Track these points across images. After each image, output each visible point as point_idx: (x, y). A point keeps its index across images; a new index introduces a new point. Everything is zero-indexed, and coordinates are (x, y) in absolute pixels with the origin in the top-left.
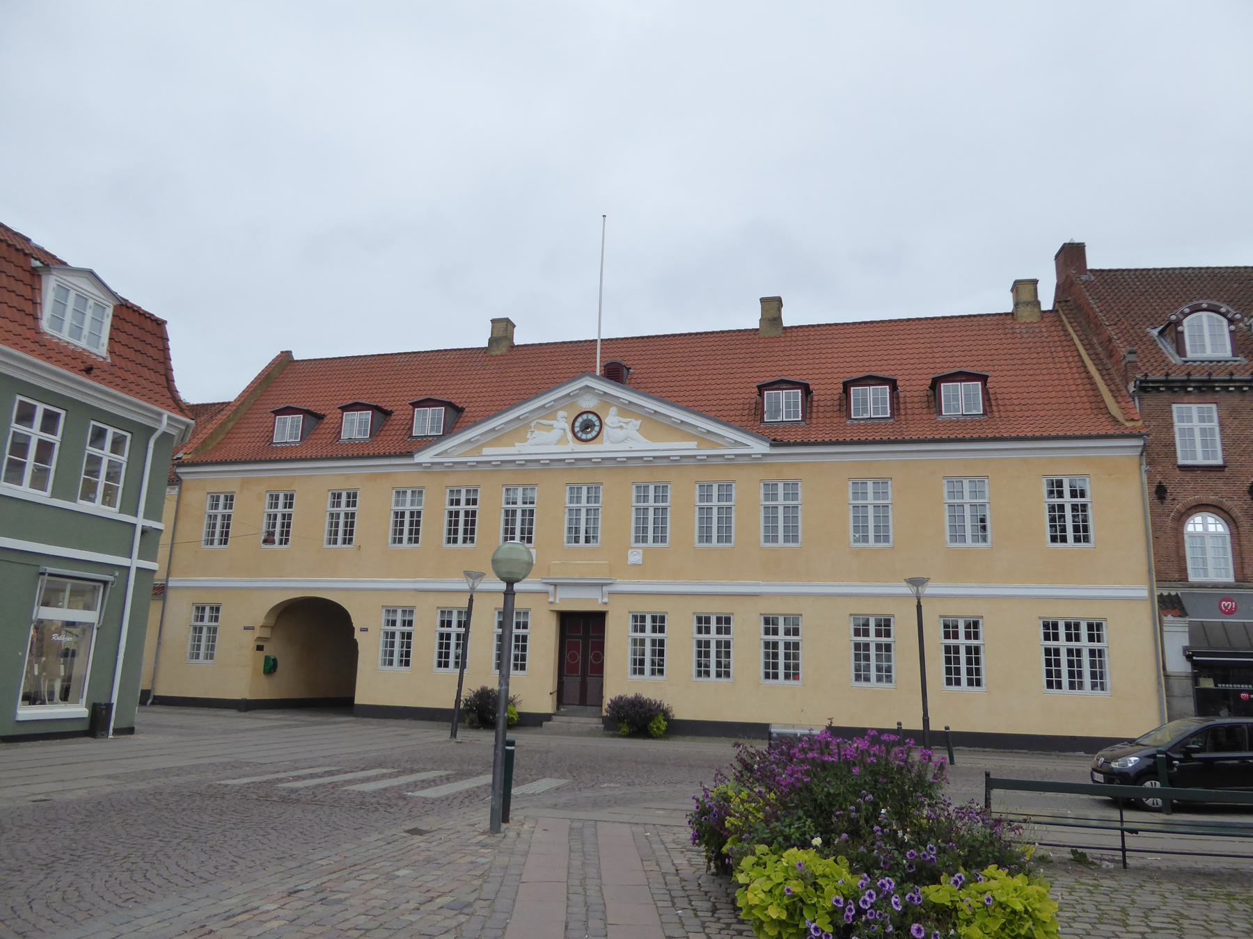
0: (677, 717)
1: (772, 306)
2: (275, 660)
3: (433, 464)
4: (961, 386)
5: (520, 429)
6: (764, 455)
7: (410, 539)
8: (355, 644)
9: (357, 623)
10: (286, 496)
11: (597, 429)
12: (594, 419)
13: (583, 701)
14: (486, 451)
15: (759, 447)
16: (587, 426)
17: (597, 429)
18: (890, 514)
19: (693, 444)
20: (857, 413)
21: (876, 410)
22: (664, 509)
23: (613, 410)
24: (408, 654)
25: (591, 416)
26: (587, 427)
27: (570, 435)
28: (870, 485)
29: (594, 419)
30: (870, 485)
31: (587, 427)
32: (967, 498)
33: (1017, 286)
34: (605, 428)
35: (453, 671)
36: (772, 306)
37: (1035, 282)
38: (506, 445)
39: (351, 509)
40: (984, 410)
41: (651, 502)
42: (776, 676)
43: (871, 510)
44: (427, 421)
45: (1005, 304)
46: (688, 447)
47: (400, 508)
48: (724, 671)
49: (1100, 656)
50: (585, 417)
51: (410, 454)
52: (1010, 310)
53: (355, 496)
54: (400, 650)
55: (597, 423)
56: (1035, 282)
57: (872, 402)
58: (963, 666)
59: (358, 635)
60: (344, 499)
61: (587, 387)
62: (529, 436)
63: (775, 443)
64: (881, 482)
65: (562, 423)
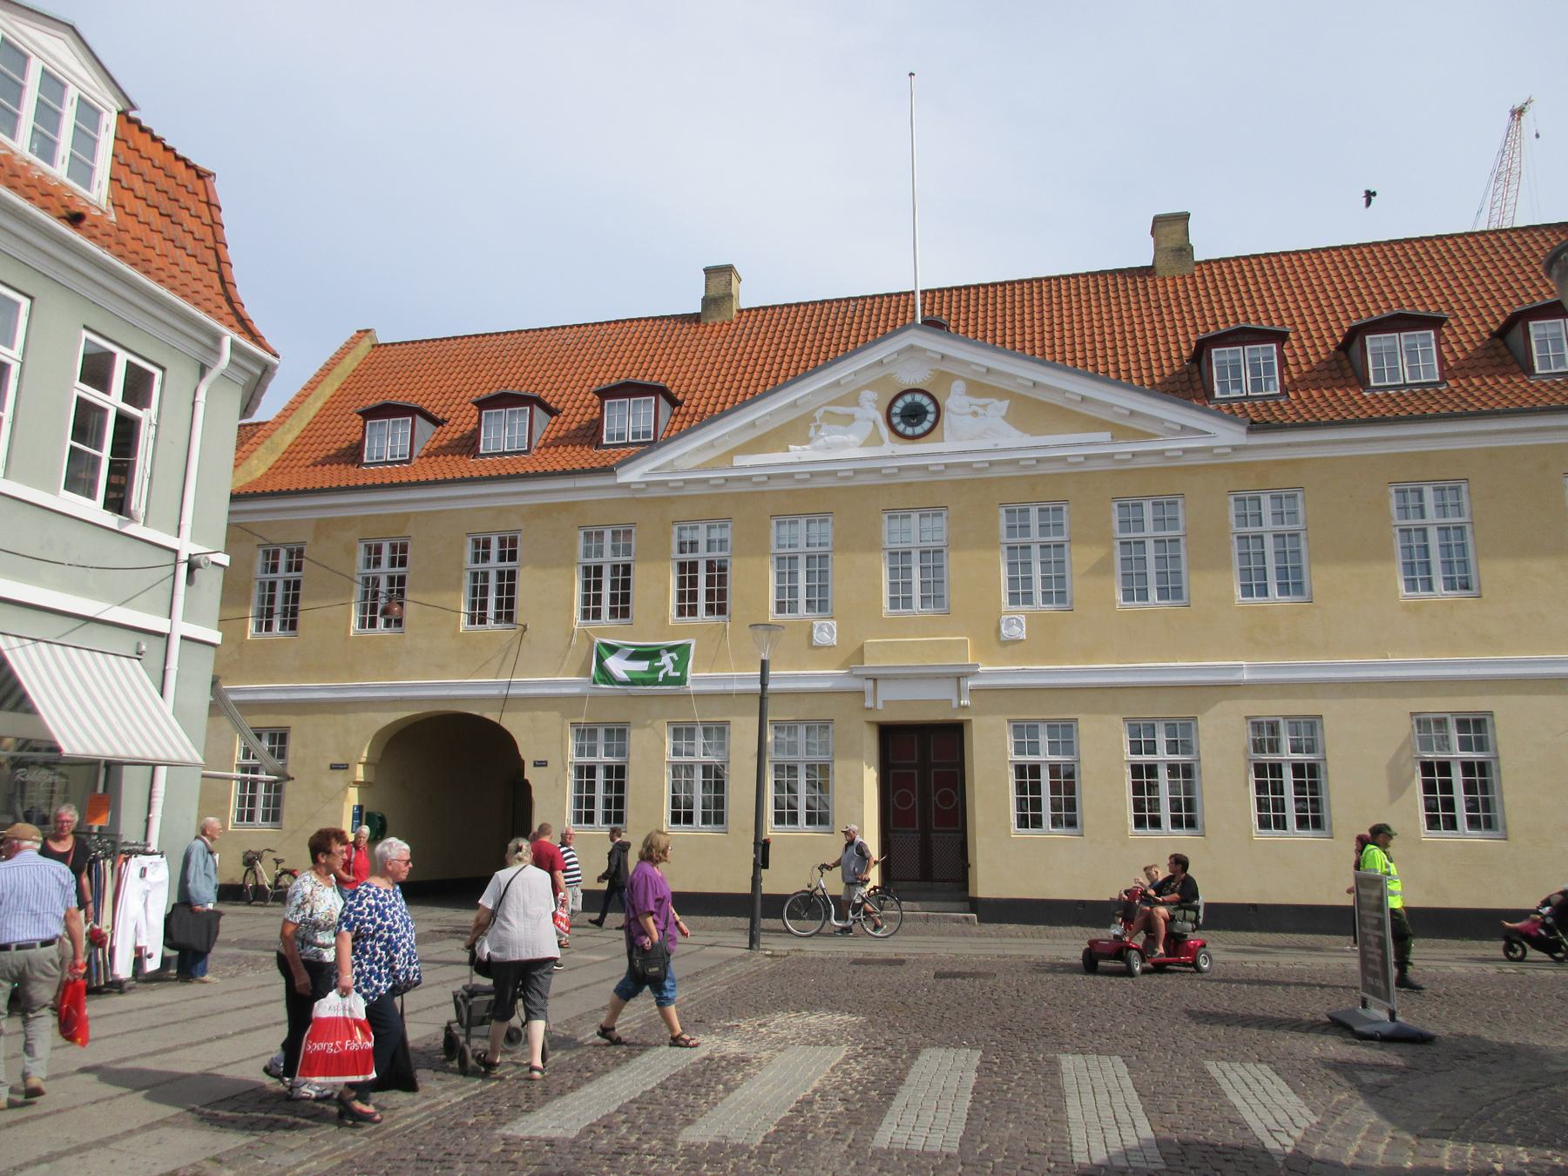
0: (980, 895)
1: (721, 276)
2: (382, 819)
3: (648, 484)
4: (1400, 339)
5: (796, 429)
6: (1235, 448)
7: (498, 616)
8: (526, 787)
9: (527, 753)
10: (393, 548)
11: (931, 417)
12: (925, 401)
13: (926, 875)
14: (739, 461)
15: (1226, 435)
16: (914, 414)
17: (931, 417)
18: (1183, 554)
19: (1105, 436)
20: (1224, 389)
21: (1256, 385)
22: (1460, 529)
23: (958, 386)
24: (620, 802)
25: (919, 398)
26: (913, 414)
27: (884, 431)
28: (1148, 506)
29: (925, 401)
30: (1148, 506)
31: (913, 414)
32: (1150, 529)
33: (1162, 224)
34: (946, 418)
35: (600, 829)
36: (721, 276)
37: (1185, 217)
38: (773, 450)
39: (294, 574)
40: (1442, 374)
41: (1035, 535)
42: (1037, 822)
43: (1150, 546)
44: (629, 419)
45: (1142, 254)
46: (1098, 442)
47: (593, 561)
48: (1067, 816)
49: (1483, 773)
50: (908, 398)
51: (608, 470)
52: (696, 307)
53: (514, 542)
54: (1050, 797)
55: (931, 408)
56: (1185, 217)
57: (1403, 361)
58: (1046, 796)
59: (530, 774)
60: (494, 549)
61: (911, 348)
62: (812, 433)
63: (1255, 427)
64: (1449, 490)
65: (870, 412)
